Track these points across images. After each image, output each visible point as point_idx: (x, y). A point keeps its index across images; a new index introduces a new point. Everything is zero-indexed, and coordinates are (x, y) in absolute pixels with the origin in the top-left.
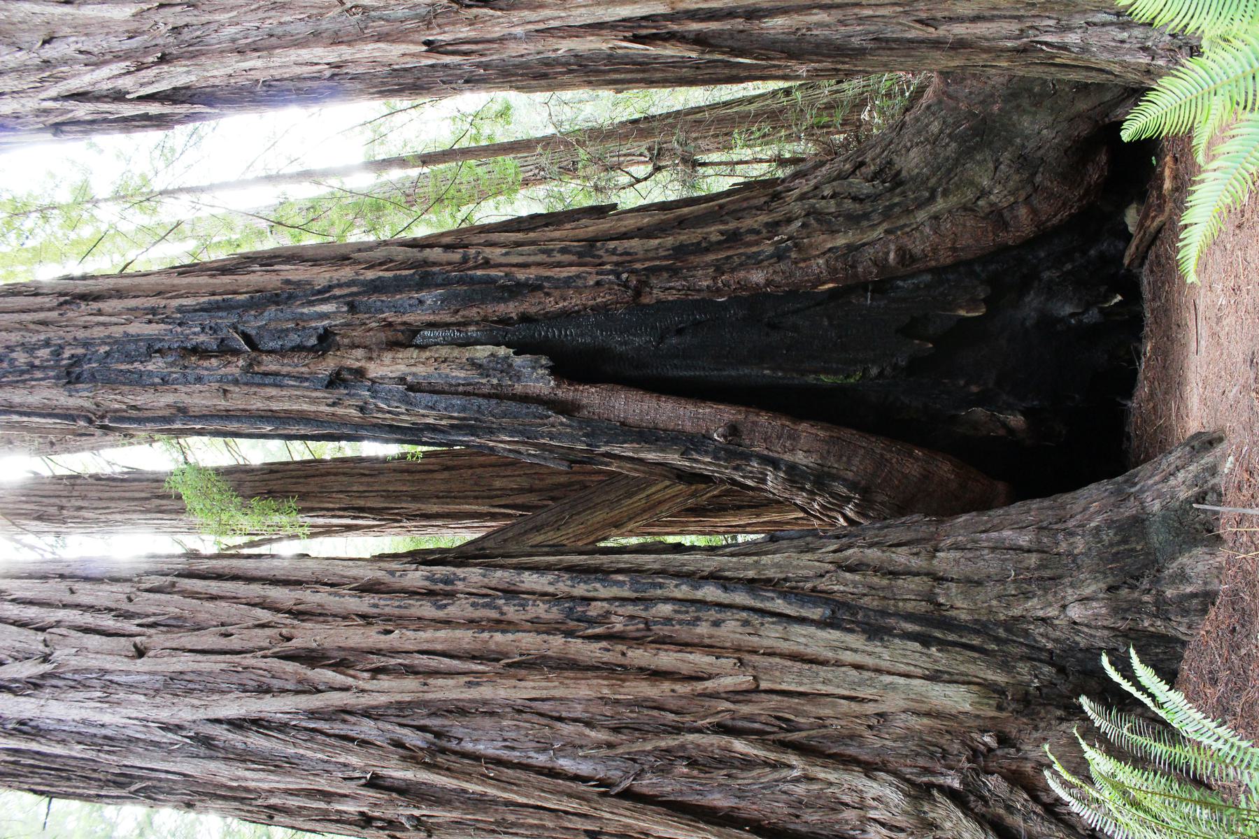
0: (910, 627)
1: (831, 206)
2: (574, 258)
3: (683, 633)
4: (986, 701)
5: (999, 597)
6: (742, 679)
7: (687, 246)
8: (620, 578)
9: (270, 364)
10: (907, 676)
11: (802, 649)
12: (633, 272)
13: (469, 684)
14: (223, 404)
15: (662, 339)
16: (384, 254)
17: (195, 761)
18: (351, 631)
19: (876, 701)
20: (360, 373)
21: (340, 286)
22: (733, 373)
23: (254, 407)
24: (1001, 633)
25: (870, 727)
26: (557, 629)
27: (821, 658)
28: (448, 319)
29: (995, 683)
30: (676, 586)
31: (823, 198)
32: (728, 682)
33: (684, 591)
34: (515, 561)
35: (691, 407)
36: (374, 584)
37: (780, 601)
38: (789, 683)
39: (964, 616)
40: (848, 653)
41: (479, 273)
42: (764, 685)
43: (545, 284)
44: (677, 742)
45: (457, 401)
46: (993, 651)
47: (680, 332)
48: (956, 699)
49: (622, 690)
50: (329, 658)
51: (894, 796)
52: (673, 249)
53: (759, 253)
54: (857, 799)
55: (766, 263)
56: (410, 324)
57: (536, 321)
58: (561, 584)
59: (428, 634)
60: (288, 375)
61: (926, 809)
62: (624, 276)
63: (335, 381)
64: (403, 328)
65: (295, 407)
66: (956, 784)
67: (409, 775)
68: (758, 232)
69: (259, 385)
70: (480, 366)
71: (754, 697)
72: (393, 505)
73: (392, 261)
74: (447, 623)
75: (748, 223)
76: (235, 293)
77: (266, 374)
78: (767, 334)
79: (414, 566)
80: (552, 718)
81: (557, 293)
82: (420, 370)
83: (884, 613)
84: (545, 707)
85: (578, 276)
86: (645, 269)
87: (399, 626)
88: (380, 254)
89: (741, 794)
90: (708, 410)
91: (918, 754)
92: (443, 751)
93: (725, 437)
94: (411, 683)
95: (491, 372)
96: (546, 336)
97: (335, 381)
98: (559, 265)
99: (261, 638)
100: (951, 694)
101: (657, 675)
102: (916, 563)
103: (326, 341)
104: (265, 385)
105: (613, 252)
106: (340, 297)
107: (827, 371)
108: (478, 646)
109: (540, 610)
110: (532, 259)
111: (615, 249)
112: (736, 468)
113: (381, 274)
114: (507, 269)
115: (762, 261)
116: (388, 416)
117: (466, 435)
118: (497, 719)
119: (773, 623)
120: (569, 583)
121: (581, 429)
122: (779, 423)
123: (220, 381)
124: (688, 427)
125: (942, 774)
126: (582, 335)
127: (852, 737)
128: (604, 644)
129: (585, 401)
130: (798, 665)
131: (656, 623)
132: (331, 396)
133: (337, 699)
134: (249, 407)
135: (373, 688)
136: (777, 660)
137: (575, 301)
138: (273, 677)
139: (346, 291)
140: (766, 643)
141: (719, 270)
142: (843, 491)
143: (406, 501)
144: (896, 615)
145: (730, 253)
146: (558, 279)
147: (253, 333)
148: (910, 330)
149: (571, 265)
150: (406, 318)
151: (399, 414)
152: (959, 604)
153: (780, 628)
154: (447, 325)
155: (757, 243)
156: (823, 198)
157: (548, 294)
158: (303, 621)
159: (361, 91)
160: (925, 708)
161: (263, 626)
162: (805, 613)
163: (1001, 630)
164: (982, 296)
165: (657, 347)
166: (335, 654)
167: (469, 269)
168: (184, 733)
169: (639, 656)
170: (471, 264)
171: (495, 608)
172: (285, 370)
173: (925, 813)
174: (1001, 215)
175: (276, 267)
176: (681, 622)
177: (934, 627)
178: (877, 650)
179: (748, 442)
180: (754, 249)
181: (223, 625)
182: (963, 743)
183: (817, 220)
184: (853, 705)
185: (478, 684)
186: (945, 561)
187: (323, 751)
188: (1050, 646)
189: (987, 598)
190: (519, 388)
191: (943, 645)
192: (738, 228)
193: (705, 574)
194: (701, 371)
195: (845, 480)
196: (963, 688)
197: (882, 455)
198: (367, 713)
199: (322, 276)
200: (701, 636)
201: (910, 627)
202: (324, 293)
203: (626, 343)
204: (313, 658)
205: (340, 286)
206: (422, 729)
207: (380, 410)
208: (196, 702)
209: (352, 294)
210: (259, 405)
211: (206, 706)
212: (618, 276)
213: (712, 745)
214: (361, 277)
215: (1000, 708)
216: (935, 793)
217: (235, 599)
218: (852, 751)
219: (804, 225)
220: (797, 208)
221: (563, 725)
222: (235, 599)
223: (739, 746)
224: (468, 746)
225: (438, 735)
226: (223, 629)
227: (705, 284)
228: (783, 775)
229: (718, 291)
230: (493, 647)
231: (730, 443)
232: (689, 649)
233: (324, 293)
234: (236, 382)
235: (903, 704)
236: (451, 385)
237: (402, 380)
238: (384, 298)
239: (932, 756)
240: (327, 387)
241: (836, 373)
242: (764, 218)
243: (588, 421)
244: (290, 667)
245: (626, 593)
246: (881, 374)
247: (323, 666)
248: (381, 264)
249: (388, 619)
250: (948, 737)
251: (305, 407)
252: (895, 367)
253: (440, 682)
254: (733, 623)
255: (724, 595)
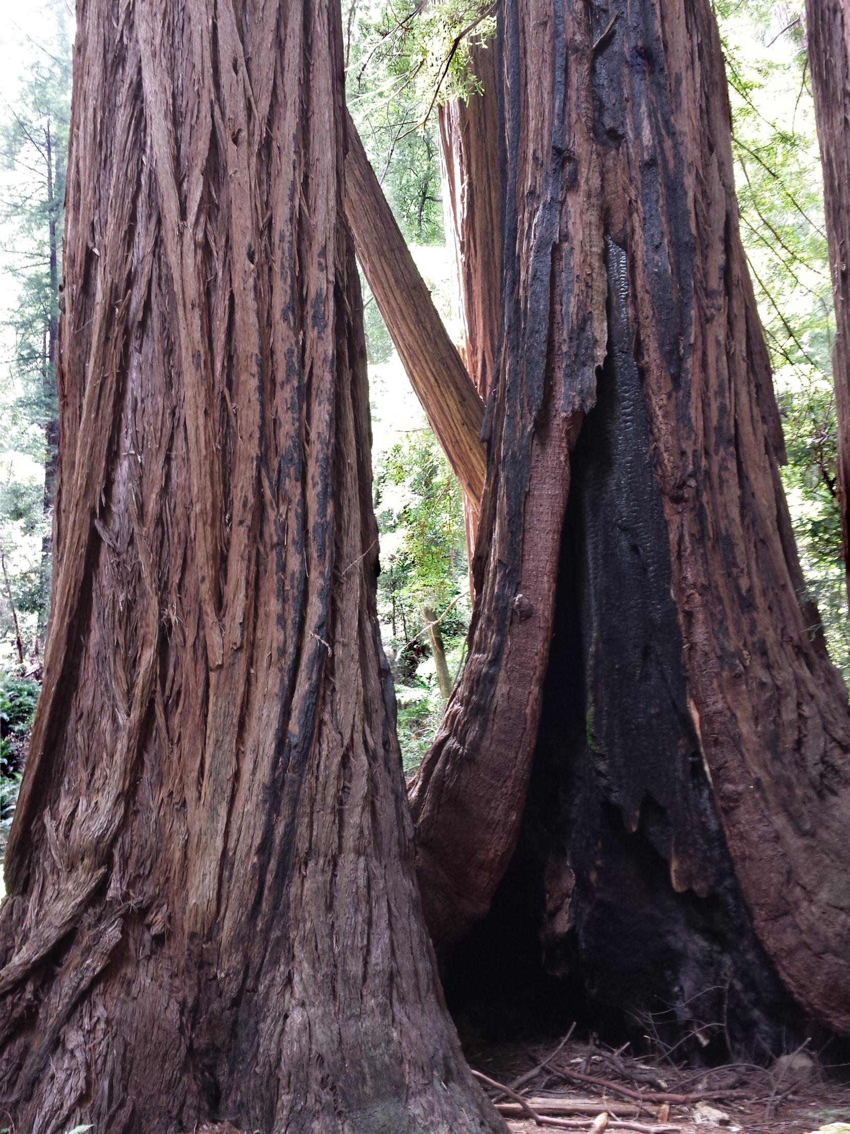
0: (280, 830)
1: (789, 715)
2: (714, 422)
3: (270, 584)
4: (199, 921)
5: (314, 931)
6: (219, 652)
7: (732, 552)
8: (330, 510)
9: (578, 75)
10: (227, 834)
11: (255, 714)
12: (698, 491)
13: (196, 356)
14: (531, 24)
15: (625, 529)
16: (717, 196)
17: (101, 49)
18: (247, 211)
19: (200, 798)
20: (572, 185)
21: (676, 145)
22: (593, 610)
23: (529, 62)
24: (275, 934)
25: (171, 794)
26: (267, 449)
27: (246, 735)
28: (639, 282)
29: (220, 929)
30: (322, 573)
31: (799, 705)
32: (214, 638)
33: (317, 582)
34: (348, 392)
35: (548, 567)
36: (308, 234)
37: (307, 686)
38: (215, 704)
39: (293, 890)
40: (251, 767)
41: (693, 313)
42: (213, 676)
43: (681, 393)
44: (148, 588)
45: (543, 305)
46: (255, 925)
47: (634, 549)
48: (201, 888)
49: (200, 524)
50: (218, 191)
51: (97, 826)
52: (728, 536)
53: (726, 632)
54: (97, 786)
55: (714, 642)
56: (632, 238)
57: (641, 386)
58: (319, 446)
59: (251, 304)
60: (566, 98)
61: (86, 861)
62: (692, 483)
63: (562, 156)
64: (628, 229)
65: (531, 112)
66: (111, 893)
67: (99, 297)
68: (752, 632)
69: (553, 64)
70: (582, 329)
71: (201, 666)
72: (478, 241)
73: (709, 204)
74: (266, 324)
75: (764, 619)
76: (663, 18)
77: (566, 70)
78: (636, 647)
79: (332, 278)
80: (170, 449)
81: (671, 408)
82: (577, 258)
83: (295, 802)
84: (179, 442)
85: (691, 429)
86: (702, 506)
87: (260, 266)
88: (717, 190)
89: (101, 660)
90: (546, 586)
91: (142, 848)
92: (127, 332)
93: (519, 606)
94: (193, 289)
95: (575, 343)
96: (624, 399)
97: (562, 156)
98: (706, 405)
99: (235, 107)
100: (207, 881)
101: (221, 561)
102: (350, 834)
103: (609, 138)
104: (553, 72)
105: (723, 468)
106: (662, 148)
107: (598, 714)
108: (242, 361)
109: (287, 427)
110: (712, 373)
111: (727, 469)
112: (489, 620)
113: (691, 194)
114: (699, 345)
115: (717, 639)
116: (526, 224)
117: (510, 320)
118: (163, 390)
119: (282, 681)
120: (321, 456)
121: (520, 449)
122: (537, 664)
123: (557, 17)
124: (529, 565)
125: (123, 877)
126: (626, 440)
127: (160, 775)
128: (251, 500)
129: (550, 450)
130: (237, 712)
131: (279, 555)
132: (545, 156)
133: (171, 206)
134: (528, 56)
135: (185, 248)
136: (242, 689)
137: (662, 426)
138: (192, 127)
139: (669, 155)
140: (261, 676)
141: (704, 589)
142: (471, 736)
143: (483, 257)
144: (293, 816)
145: (726, 602)
146: (687, 407)
147: (616, 48)
148: (649, 804)
149: (706, 419)
150: (638, 231)
151: (528, 238)
152: (307, 885)
153: (276, 690)
154: (632, 281)
155: (739, 631)
156: (799, 705)
157: (669, 396)
158: (259, 154)
159: (832, 136)
160: (191, 853)
161: (249, 109)
162: (295, 714)
163: (278, 933)
164: (696, 888)
165: (615, 525)
166: (223, 198)
167: (699, 299)
168: (126, 32)
169: (239, 538)
170: (705, 302)
171: (288, 376)
172: (572, 93)
173: (83, 859)
174: (786, 913)
175: (697, 64)
176: (282, 583)
177: (280, 859)
178: (254, 798)
179: (515, 630)
180: (731, 629)
181: (248, 61)
182: (154, 898)
183: (769, 700)
184: (195, 774)
185: (198, 366)
186: (352, 869)
187: (116, 197)
188: (261, 988)
189: (312, 918)
190: (559, 374)
191: (262, 869)
192: (756, 608)
193: (339, 603)
194: (594, 578)
195: (481, 738)
196: (212, 894)
197: (510, 776)
198: (159, 242)
199: (686, 123)
200: (266, 604)
201: (280, 830)
202: (665, 128)
203: (619, 490)
204: (216, 171)
205: (676, 145)
206: (147, 307)
207: (532, 215)
208: (157, 41)
209: (665, 160)
210: (532, 68)
211: (154, 55)
212: (693, 475)
213: (147, 625)
214: (686, 171)
215: (193, 936)
216: (102, 870)
217: (279, 69)
218: (146, 776)
219: (762, 685)
220: (784, 676)
221: (161, 463)
222: (279, 69)
223: (148, 655)
224: (135, 359)
225: (143, 325)
226: (241, 61)
227: (689, 575)
228: (120, 704)
229: (681, 591)
230: (242, 378)
231: (513, 610)
232: (251, 593)
233: (665, 128)
234: (556, 35)
235: (195, 830)
236: (561, 296)
237: (565, 237)
238: (661, 202)
239: (140, 863)
240: (554, 148)
241: (597, 724)
242: (771, 637)
243: (528, 457)
244: (203, 146)
245: (312, 520)
246: (599, 773)
247: (206, 185)
248: (704, 192)
249: (269, 252)
250: (162, 880)
251: (532, 124)
252: (608, 789)
253: (197, 322)
254: (282, 637)
255: (313, 625)
